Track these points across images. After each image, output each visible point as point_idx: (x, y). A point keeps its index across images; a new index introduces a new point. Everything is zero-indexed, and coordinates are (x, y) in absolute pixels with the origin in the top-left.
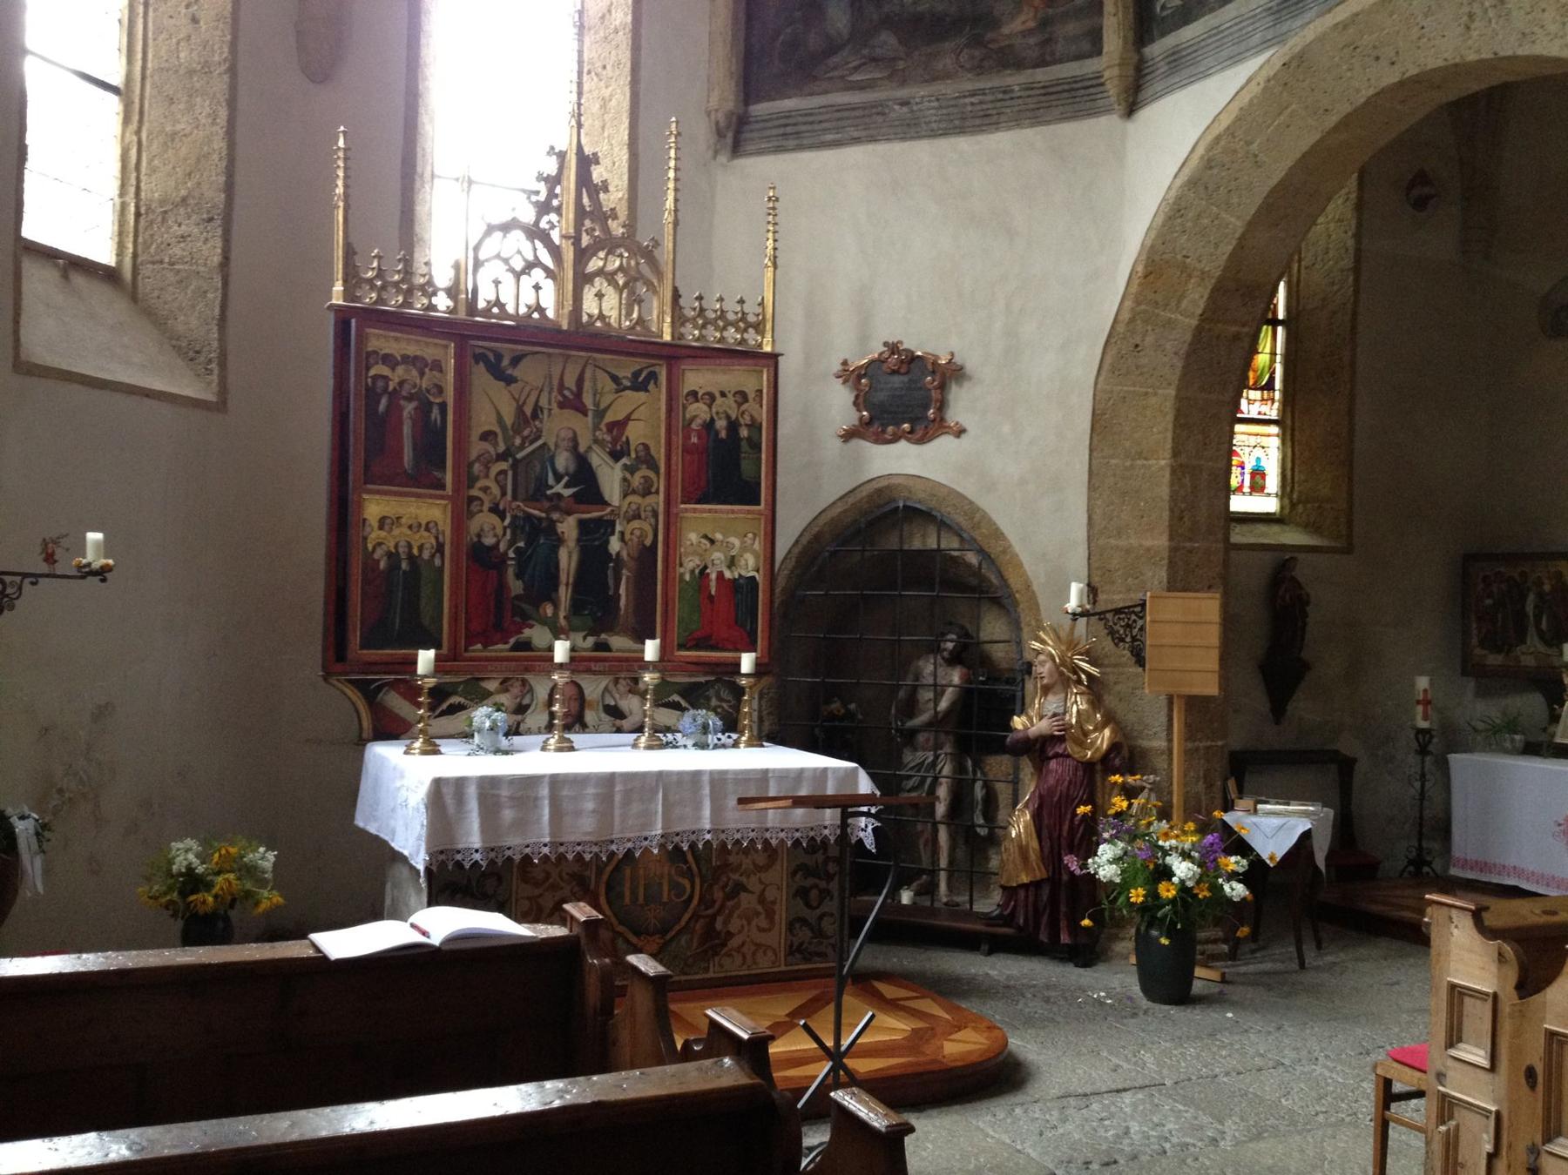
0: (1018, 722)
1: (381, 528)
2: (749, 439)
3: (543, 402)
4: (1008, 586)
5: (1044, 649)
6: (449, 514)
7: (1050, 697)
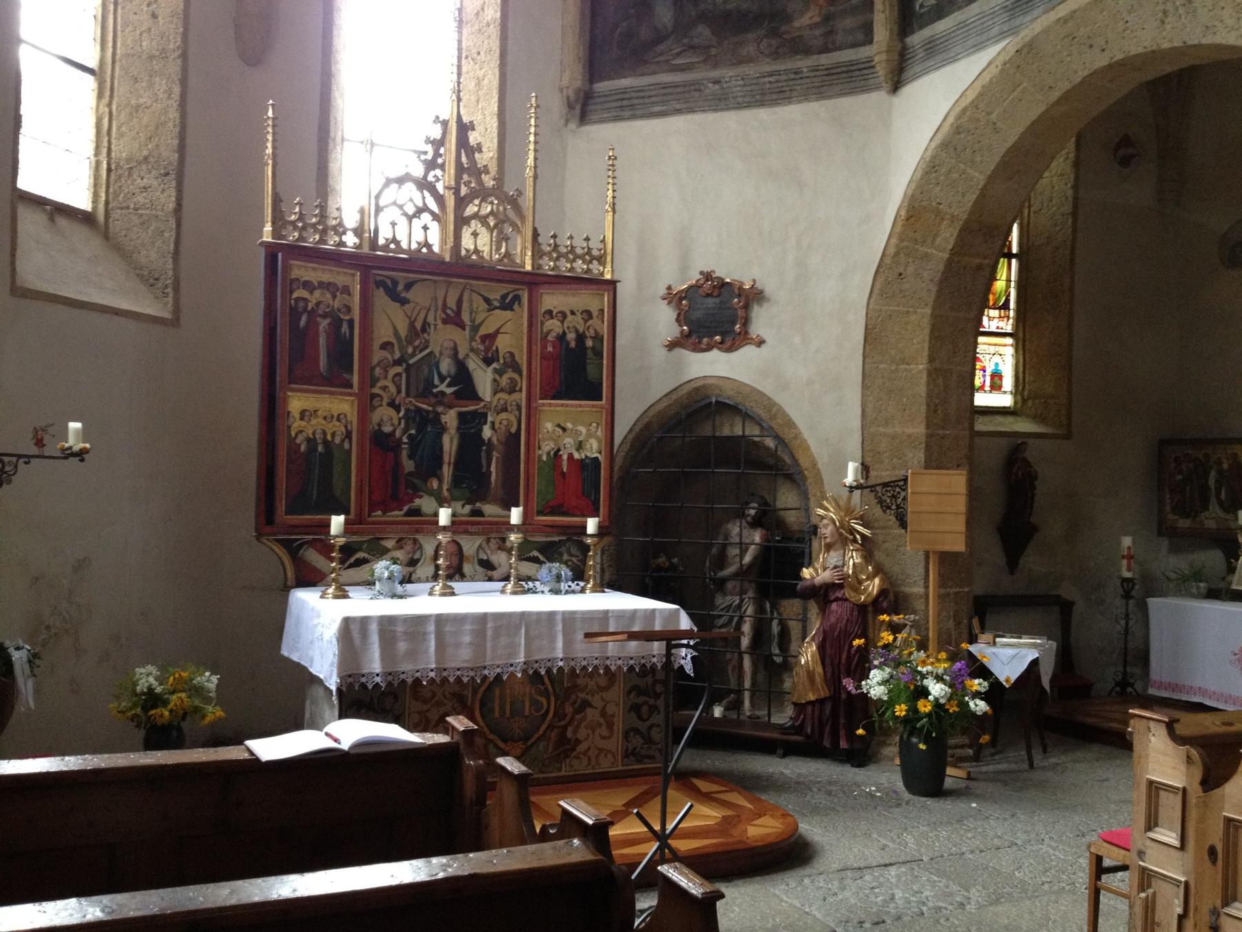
0: (806, 573)
1: (302, 419)
2: (593, 348)
3: (430, 319)
4: (798, 465)
5: (827, 515)
6: (356, 408)
7: (832, 553)
